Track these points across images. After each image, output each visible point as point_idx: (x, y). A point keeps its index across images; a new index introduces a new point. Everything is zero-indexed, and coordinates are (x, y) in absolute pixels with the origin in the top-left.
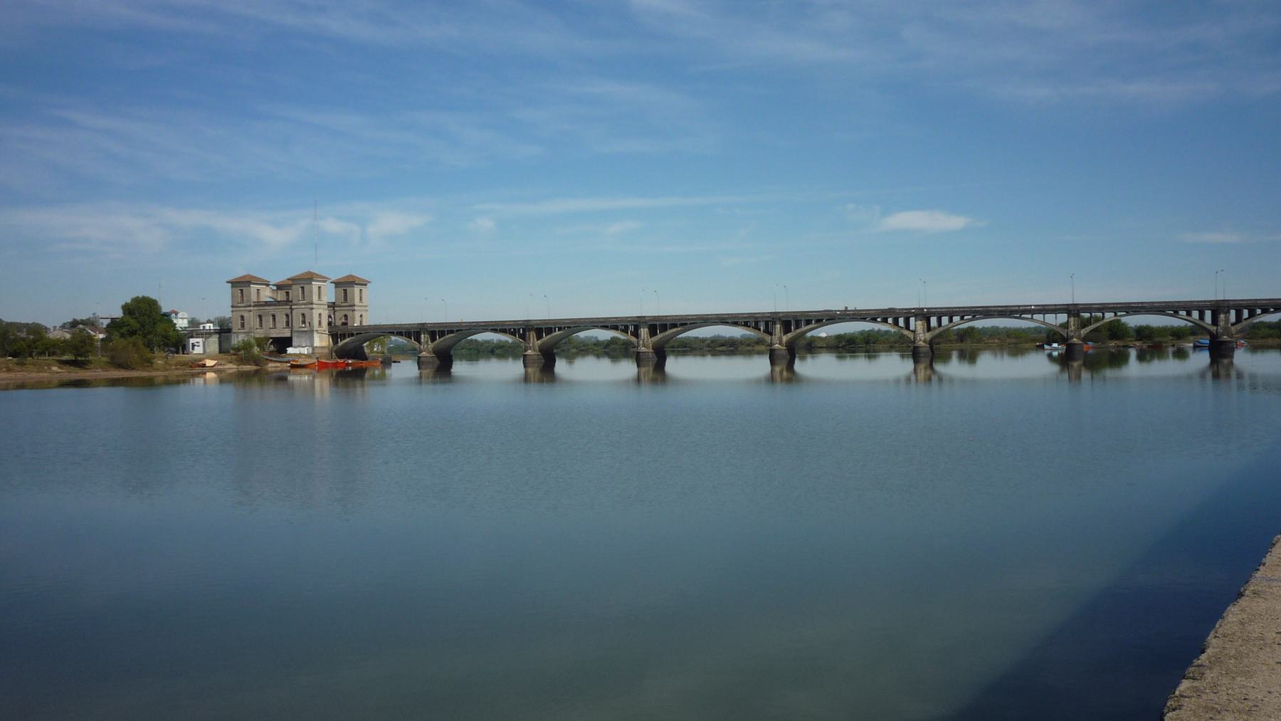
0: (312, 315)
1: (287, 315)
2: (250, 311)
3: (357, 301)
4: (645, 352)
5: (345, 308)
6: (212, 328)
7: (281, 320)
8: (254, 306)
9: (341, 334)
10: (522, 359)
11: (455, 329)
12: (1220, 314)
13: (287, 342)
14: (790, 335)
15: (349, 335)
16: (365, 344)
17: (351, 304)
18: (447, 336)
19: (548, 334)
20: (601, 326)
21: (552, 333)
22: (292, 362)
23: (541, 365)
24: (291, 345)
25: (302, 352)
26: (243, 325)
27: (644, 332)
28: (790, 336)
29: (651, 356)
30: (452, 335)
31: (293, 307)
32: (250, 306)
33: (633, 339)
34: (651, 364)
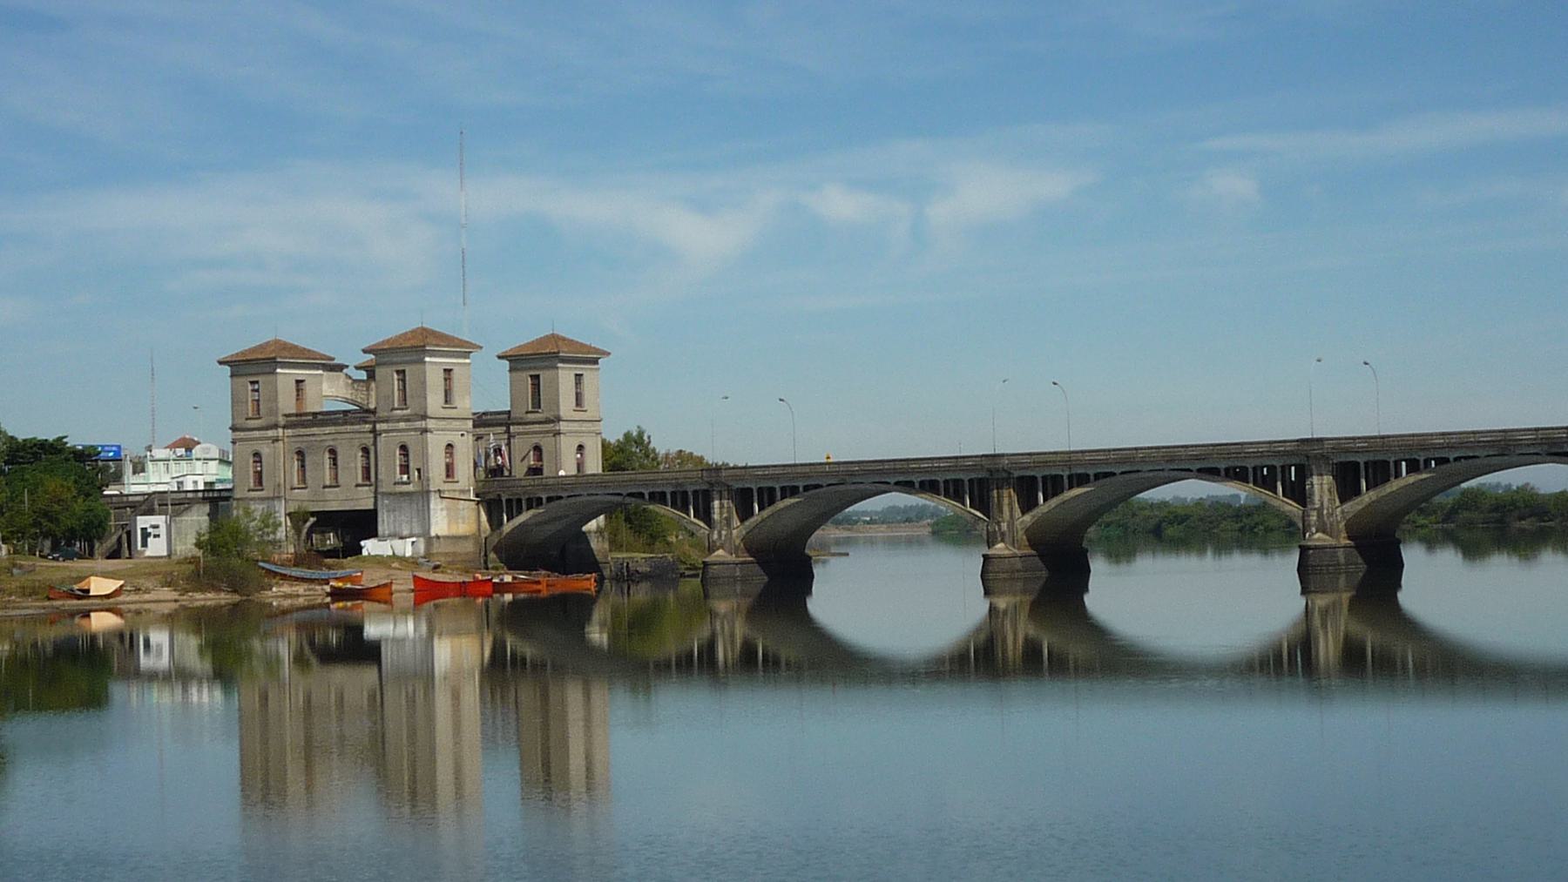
0: (424, 446)
1: (365, 450)
2: (276, 440)
3: (566, 406)
4: (1324, 547)
5: (537, 427)
7: (352, 463)
8: (284, 427)
9: (509, 501)
10: (1295, 557)
11: (801, 484)
12: (713, 501)
13: (362, 524)
15: (529, 500)
16: (592, 525)
17: (550, 415)
18: (780, 505)
19: (1055, 494)
20: (1199, 470)
21: (1386, 480)
22: (332, 583)
23: (1038, 586)
24: (373, 533)
25: (399, 553)
26: (259, 477)
27: (1321, 486)
29: (1342, 560)
31: (378, 426)
32: (276, 426)
33: (1291, 508)
34: (1342, 580)
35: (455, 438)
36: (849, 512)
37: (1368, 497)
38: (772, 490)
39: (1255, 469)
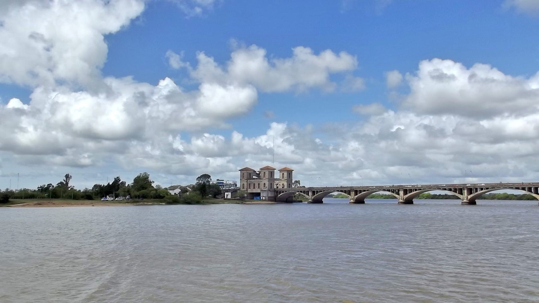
6: (235, 188)
14: (472, 195)
18: (319, 193)
19: (360, 193)
27: (401, 193)
28: (472, 196)
30: (321, 193)
35: (265, 182)
36: (331, 194)
37: (409, 195)
38: (318, 191)
39: (391, 190)
